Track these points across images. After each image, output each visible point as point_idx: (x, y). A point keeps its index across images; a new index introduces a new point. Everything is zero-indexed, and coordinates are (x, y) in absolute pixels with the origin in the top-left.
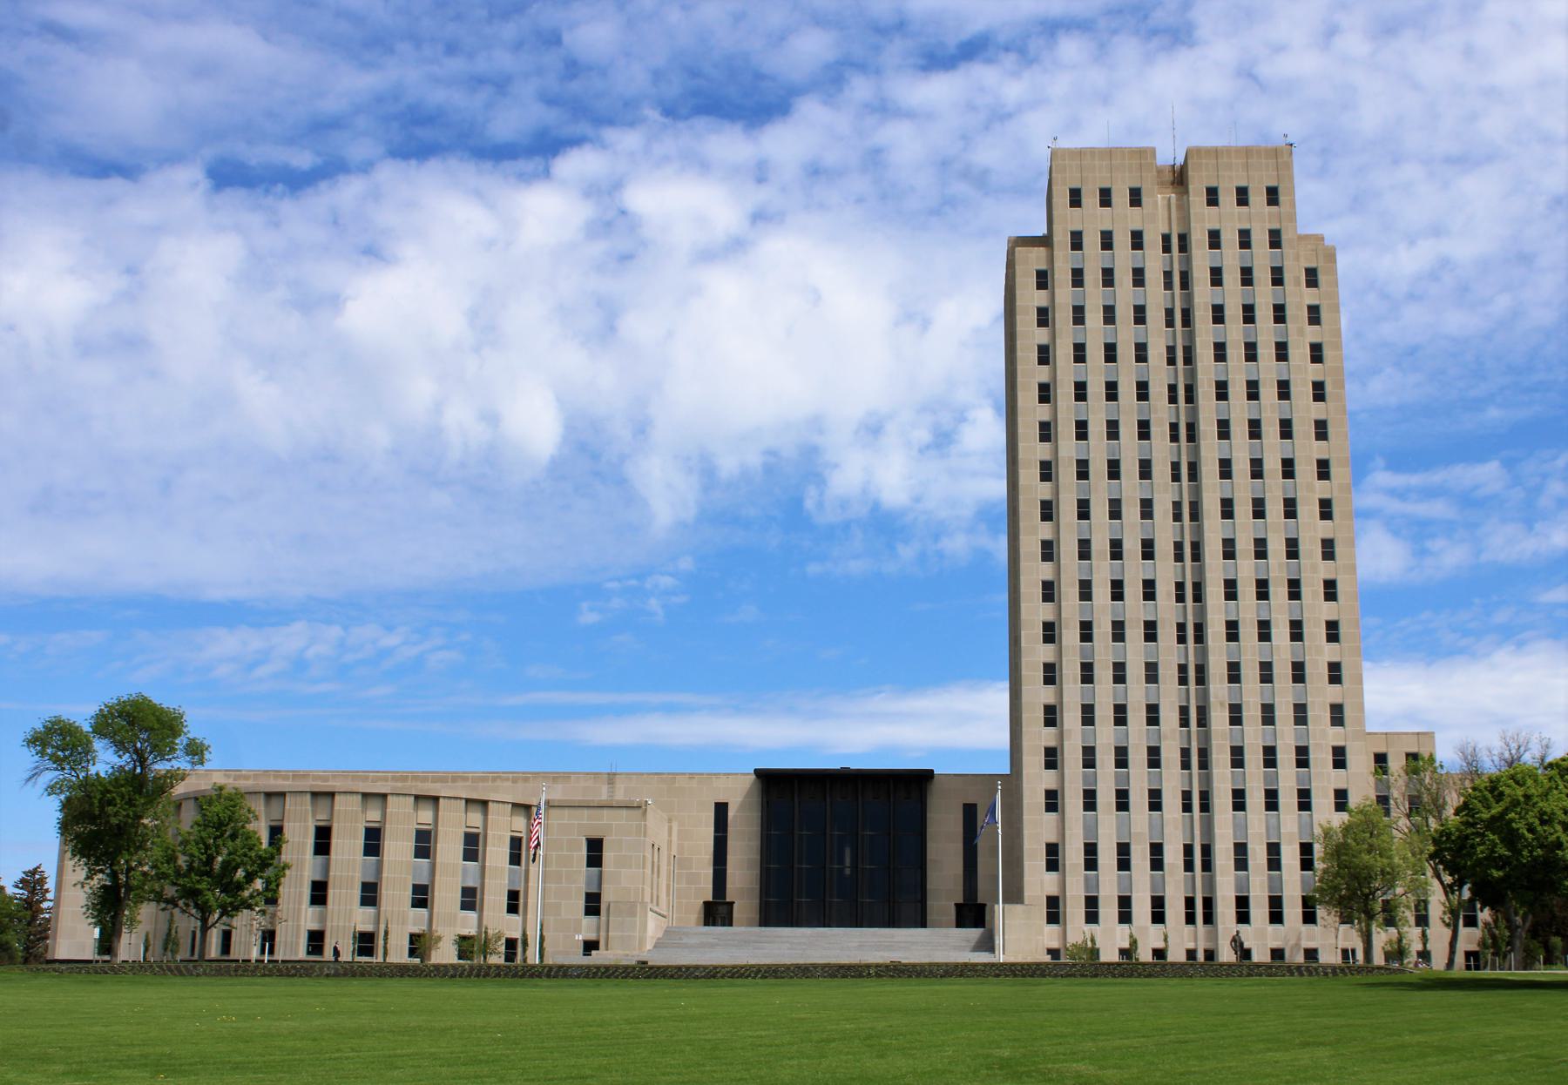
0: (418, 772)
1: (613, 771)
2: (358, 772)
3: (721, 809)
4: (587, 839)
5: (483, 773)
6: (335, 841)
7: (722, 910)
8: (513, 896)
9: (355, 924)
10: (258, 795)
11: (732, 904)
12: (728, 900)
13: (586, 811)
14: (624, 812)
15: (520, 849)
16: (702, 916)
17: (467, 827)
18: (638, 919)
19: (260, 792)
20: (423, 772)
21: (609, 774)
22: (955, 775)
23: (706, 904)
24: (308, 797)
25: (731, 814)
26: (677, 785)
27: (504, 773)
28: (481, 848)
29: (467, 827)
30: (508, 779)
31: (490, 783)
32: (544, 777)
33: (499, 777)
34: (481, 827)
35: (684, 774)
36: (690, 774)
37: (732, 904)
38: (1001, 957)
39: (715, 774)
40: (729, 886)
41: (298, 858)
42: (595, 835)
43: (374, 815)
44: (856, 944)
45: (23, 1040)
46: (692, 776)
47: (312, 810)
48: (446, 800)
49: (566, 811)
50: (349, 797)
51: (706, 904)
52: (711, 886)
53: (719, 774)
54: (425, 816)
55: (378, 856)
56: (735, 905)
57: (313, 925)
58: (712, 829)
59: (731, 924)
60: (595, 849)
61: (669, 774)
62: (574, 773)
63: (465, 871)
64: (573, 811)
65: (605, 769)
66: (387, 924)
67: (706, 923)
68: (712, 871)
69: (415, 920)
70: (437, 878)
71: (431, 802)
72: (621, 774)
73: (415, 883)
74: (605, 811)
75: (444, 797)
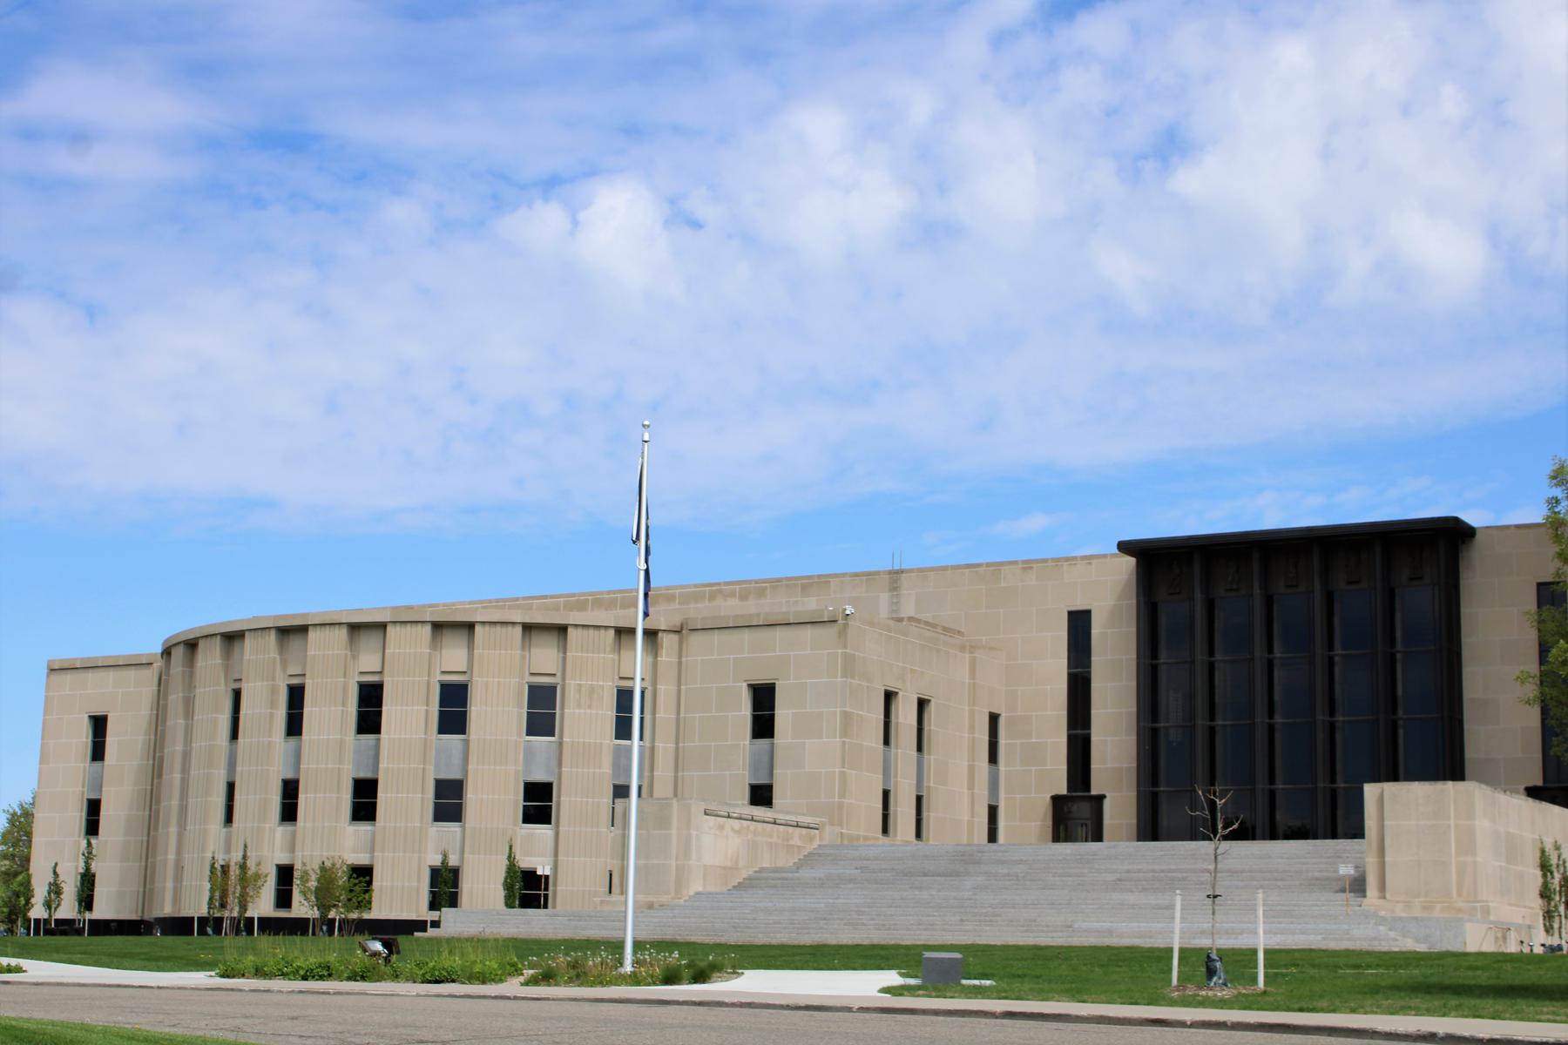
0: (602, 593)
1: (897, 567)
2: (517, 599)
3: (1079, 623)
4: (750, 686)
5: (696, 586)
6: (388, 709)
7: (1082, 810)
8: (290, 790)
9: (214, 853)
10: (214, 637)
11: (1101, 798)
12: (1094, 792)
13: (747, 635)
14: (809, 632)
15: (630, 710)
16: (1049, 823)
17: (621, 678)
18: (674, 831)
19: (216, 634)
20: (609, 592)
21: (890, 572)
22: (1518, 527)
23: (1057, 800)
24: (273, 635)
25: (1096, 630)
26: (1003, 585)
27: (727, 583)
28: (558, 711)
29: (621, 678)
30: (733, 594)
31: (707, 604)
32: (787, 586)
33: (720, 591)
34: (559, 674)
35: (1015, 563)
36: (1024, 562)
37: (1101, 798)
38: (375, 914)
39: (1068, 559)
40: (1095, 765)
41: (259, 742)
42: (762, 678)
43: (368, 662)
44: (1111, 877)
45: (215, 1032)
46: (1027, 565)
47: (281, 659)
48: (487, 628)
49: (716, 637)
50: (327, 632)
51: (1057, 800)
52: (1065, 767)
53: (1075, 558)
54: (544, 657)
55: (465, 734)
56: (1107, 804)
57: (282, 855)
58: (1065, 661)
59: (1098, 836)
60: (763, 697)
61: (988, 565)
62: (836, 575)
63: (529, 753)
64: (726, 635)
65: (883, 564)
66: (245, 851)
67: (1056, 838)
68: (1065, 740)
69: (440, 841)
70: (471, 767)
71: (555, 634)
72: (911, 571)
73: (617, 782)
74: (779, 633)
75: (484, 623)
